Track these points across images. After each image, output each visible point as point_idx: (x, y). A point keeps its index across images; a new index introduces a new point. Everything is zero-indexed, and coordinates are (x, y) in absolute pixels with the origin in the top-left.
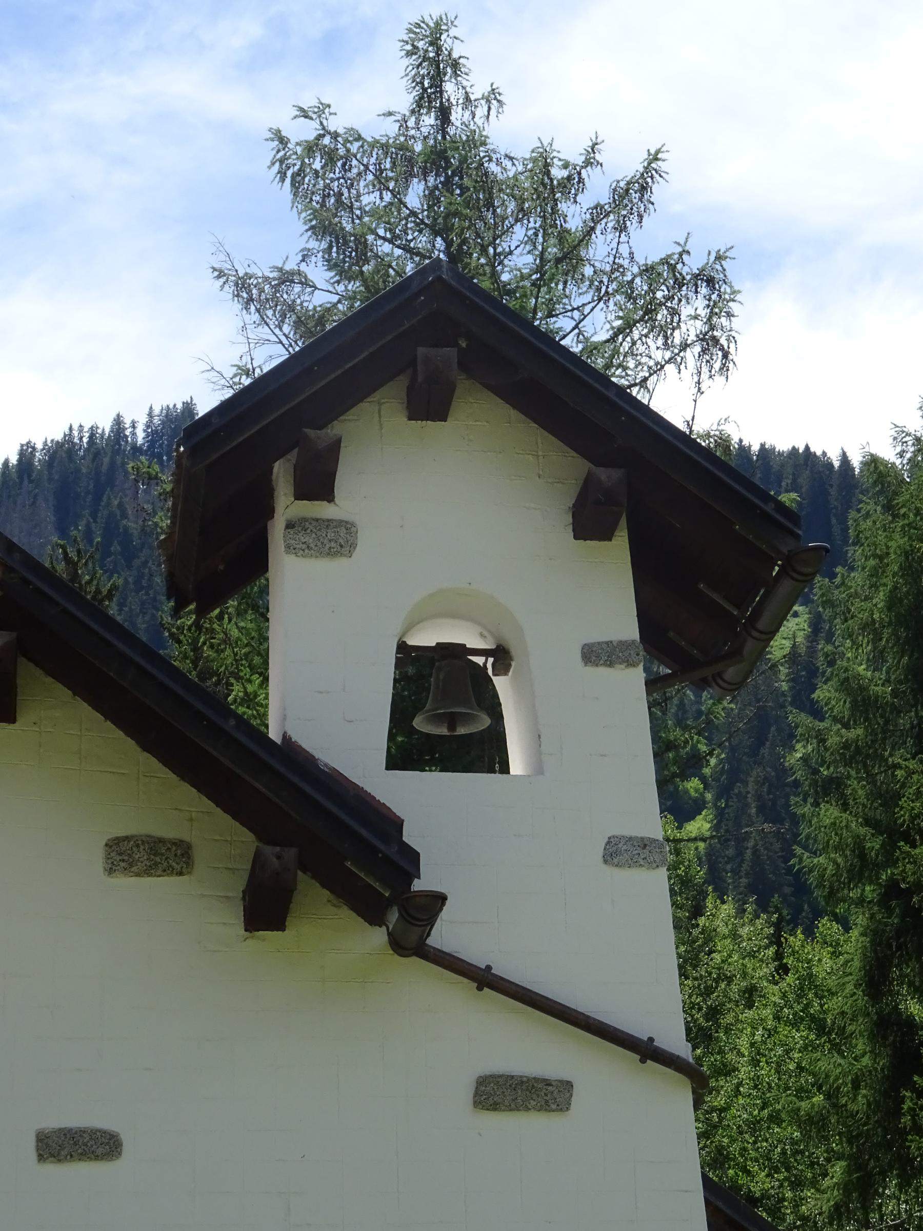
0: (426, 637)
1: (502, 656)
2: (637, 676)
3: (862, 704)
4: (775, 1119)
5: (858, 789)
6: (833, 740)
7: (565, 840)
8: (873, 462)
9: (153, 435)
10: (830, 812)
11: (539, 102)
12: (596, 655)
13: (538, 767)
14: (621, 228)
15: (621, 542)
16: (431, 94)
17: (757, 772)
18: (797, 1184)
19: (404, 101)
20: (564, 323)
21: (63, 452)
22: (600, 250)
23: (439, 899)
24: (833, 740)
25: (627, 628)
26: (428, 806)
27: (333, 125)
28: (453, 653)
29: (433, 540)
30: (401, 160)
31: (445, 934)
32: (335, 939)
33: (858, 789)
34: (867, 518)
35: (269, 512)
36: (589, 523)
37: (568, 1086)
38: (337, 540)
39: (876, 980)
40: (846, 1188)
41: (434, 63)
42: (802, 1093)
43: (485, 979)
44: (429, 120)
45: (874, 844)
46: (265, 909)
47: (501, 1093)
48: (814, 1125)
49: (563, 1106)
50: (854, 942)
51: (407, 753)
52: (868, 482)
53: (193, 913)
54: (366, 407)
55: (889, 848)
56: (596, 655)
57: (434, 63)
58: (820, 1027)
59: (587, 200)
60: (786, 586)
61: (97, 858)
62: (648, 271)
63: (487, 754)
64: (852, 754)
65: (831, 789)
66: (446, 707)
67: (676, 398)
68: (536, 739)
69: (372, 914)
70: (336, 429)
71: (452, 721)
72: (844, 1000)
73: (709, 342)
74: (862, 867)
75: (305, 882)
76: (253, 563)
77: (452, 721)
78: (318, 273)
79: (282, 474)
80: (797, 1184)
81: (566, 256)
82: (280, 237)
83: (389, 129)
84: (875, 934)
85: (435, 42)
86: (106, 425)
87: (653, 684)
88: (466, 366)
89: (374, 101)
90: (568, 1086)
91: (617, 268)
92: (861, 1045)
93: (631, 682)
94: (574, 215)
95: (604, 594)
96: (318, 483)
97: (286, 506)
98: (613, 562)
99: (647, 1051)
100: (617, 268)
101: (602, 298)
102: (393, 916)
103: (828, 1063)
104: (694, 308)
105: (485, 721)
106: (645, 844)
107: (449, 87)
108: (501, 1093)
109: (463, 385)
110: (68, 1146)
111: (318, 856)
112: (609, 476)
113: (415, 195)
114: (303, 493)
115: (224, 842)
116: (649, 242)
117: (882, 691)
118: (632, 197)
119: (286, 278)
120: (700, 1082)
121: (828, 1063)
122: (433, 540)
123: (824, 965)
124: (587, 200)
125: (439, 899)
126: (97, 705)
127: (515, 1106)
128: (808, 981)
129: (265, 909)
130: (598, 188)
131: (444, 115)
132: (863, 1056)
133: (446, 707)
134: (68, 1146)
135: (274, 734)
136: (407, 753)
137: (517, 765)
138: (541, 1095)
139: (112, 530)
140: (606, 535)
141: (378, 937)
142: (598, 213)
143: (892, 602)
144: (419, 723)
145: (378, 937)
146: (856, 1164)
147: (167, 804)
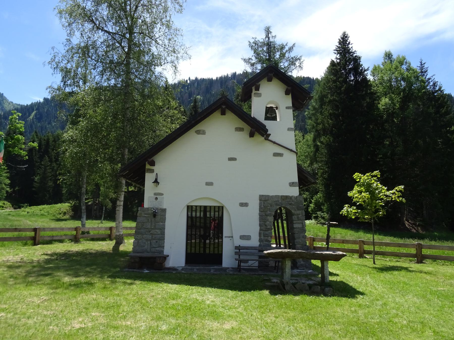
0: (269, 106)
1: (277, 108)
2: (292, 110)
3: (314, 108)
4: (302, 156)
5: (313, 118)
6: (311, 113)
7: (283, 127)
8: (317, 79)
9: (231, 76)
10: (310, 121)
11: (281, 37)
12: (287, 108)
13: (280, 120)
14: (289, 53)
15: (290, 95)
16: (267, 36)
17: (301, 115)
18: (304, 163)
19: (264, 37)
20: (282, 64)
21: (221, 78)
22: (287, 55)
23: (270, 134)
24: (311, 113)
25: (291, 105)
26: (269, 124)
27: (256, 40)
28: (272, 107)
29: (270, 95)
30: (264, 44)
31: (270, 138)
32: (259, 138)
33: (313, 118)
34: (316, 87)
35: (252, 92)
36: (287, 93)
37: (283, 154)
38: (259, 95)
39: (314, 140)
40: (310, 164)
41: (268, 31)
42: (305, 153)
43: (274, 143)
44: (267, 39)
45: (315, 125)
46: (252, 135)
47: (276, 155)
48: (306, 157)
49: (282, 156)
50: (312, 136)
51: (267, 118)
52: (316, 81)
53: (244, 135)
54: (263, 80)
55: (317, 126)
56: (287, 108)
57: (268, 31)
58: (308, 146)
59: (285, 50)
60: (308, 100)
61: (234, 129)
62: (292, 58)
63: (275, 119)
64: (313, 114)
65: (310, 118)
66: (271, 113)
67: (295, 73)
68: (280, 117)
69: (263, 136)
70: (259, 83)
71: (271, 115)
72: (310, 143)
73: (300, 66)
74: (313, 127)
75: (256, 133)
76: (250, 97)
77: (271, 115)
78: (254, 58)
79: (253, 88)
80: (304, 163)
81: (283, 56)
82: (250, 54)
83: (262, 40)
84: (315, 135)
85: (268, 30)
86: (226, 75)
87: (293, 111)
88: (274, 76)
89: (261, 37)
90: (283, 154)
91: (289, 57)
92: (312, 148)
93: (291, 111)
94: (284, 51)
95: (288, 101)
96: (257, 89)
97: (254, 91)
98: (290, 97)
99: (291, 151)
100: (289, 57)
101: (287, 61)
102: (265, 136)
103: (308, 150)
104: (297, 63)
105: (275, 115)
106: (292, 128)
107: (270, 35)
108: (276, 155)
109: (274, 78)
110: (231, 159)
111: (257, 129)
112: (289, 88)
113: (265, 49)
114: (255, 90)
115: (247, 128)
116: (292, 54)
117: (317, 107)
118: (291, 49)
119: (250, 59)
120: (297, 154)
121: (308, 150)
122: (270, 95)
123: (309, 138)
124: (285, 50)
125: (270, 134)
126: (235, 114)
127: (277, 156)
128: (307, 140)
129: (252, 135)
130: (287, 48)
131: (269, 38)
132: (313, 149)
133: (271, 113)
134: (231, 159)
135: (252, 116)
136: (267, 118)
137: (278, 120)
138: (280, 155)
139: (227, 87)
140: (289, 95)
141: (263, 138)
142: (287, 51)
143: (319, 96)
144: (268, 115)
145: (263, 138)
146: (311, 161)
147: (242, 124)
